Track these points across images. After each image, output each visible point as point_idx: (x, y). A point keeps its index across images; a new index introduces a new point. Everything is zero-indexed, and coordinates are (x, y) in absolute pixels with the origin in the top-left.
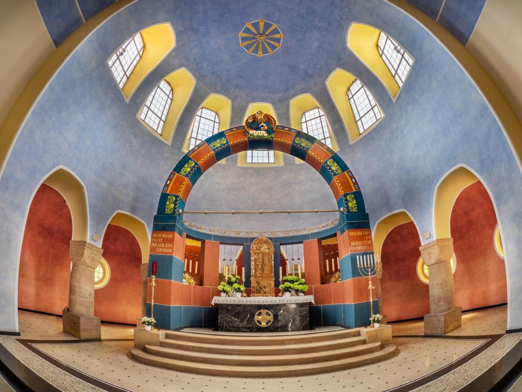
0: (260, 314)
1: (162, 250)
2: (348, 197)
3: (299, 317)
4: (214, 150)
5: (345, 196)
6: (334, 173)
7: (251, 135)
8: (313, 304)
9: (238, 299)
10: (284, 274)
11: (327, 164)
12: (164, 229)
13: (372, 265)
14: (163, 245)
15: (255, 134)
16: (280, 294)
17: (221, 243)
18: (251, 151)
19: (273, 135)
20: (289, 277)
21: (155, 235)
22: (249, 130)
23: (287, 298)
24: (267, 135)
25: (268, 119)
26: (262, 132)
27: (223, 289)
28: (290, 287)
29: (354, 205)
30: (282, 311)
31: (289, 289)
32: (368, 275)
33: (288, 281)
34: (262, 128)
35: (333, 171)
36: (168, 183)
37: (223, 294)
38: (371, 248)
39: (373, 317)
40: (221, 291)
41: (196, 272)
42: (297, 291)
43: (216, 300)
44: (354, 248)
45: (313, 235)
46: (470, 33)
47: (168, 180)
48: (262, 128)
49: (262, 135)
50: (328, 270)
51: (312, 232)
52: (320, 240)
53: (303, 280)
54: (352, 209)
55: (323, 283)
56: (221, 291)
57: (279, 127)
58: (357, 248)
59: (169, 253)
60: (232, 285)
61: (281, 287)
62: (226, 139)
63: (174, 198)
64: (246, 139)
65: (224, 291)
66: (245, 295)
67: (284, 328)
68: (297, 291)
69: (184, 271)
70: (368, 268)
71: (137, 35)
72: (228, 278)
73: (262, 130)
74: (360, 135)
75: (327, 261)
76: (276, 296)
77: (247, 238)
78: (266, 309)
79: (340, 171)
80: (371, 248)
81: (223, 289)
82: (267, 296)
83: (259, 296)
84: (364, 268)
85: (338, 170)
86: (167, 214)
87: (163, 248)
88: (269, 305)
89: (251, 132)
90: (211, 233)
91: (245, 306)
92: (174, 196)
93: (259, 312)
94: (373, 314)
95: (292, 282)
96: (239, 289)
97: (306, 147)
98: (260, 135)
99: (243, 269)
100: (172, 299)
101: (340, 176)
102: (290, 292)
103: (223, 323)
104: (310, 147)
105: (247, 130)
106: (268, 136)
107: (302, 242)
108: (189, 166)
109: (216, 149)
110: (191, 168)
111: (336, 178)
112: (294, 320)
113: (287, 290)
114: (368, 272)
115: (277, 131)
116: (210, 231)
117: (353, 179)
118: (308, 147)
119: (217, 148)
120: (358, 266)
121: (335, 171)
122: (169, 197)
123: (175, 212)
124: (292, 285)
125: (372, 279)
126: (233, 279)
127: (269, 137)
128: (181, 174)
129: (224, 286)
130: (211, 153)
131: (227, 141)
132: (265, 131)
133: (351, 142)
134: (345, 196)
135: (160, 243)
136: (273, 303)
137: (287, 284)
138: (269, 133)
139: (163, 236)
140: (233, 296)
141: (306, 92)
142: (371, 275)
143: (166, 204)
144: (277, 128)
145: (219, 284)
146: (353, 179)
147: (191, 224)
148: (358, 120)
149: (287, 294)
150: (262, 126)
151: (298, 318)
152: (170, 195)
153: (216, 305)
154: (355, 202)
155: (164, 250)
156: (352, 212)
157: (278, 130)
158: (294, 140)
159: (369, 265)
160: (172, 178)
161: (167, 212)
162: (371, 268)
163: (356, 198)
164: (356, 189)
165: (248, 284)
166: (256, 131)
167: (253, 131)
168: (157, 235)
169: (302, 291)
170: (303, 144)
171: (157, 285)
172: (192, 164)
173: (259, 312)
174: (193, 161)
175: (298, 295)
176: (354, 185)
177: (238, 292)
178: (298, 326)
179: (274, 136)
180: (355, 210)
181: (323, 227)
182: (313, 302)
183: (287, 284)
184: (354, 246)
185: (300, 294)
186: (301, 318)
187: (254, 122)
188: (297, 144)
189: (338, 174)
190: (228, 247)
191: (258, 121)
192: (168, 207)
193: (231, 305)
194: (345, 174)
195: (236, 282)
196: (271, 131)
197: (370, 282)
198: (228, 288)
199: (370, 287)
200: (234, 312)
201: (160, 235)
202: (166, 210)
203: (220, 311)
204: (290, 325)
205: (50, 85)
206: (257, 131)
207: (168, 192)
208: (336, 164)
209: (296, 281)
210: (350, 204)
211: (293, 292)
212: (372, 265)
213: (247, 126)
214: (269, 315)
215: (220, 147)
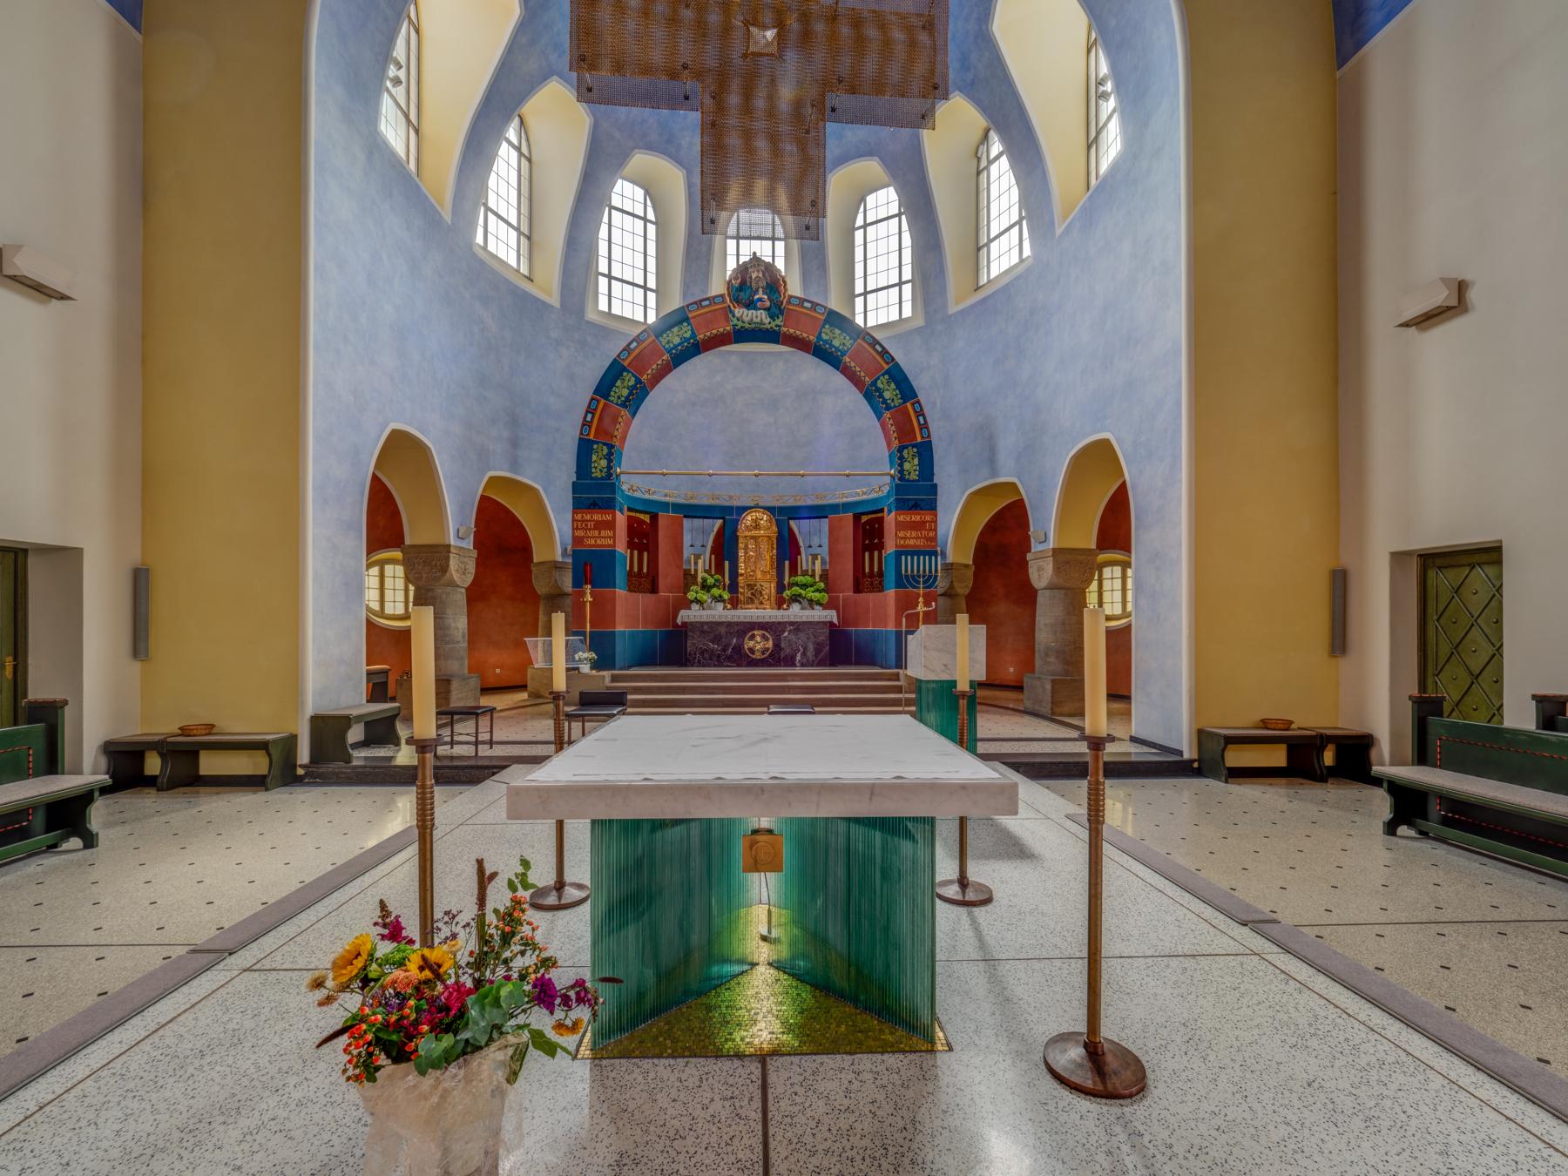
0: (752, 637)
1: (596, 541)
4: (669, 351)
6: (887, 404)
8: (835, 625)
9: (719, 613)
10: (794, 571)
11: (876, 387)
12: (594, 505)
13: (927, 572)
14: (596, 533)
15: (746, 319)
16: (785, 606)
17: (685, 517)
19: (778, 322)
20: (800, 579)
21: (579, 517)
22: (734, 307)
23: (795, 613)
24: (769, 320)
25: (774, 283)
26: (759, 312)
27: (696, 598)
28: (800, 595)
29: (914, 468)
30: (786, 634)
31: (798, 598)
32: (919, 588)
33: (797, 584)
34: (759, 304)
35: (885, 401)
36: (589, 419)
37: (695, 607)
38: (933, 544)
40: (692, 602)
41: (645, 570)
43: (684, 616)
44: (902, 542)
47: (587, 412)
48: (759, 304)
49: (758, 320)
50: (867, 570)
51: (845, 500)
52: (857, 517)
54: (910, 474)
55: (858, 589)
56: (692, 602)
57: (792, 300)
58: (908, 542)
59: (609, 546)
60: (708, 591)
61: (787, 593)
62: (689, 327)
63: (605, 450)
64: (728, 328)
65: (697, 601)
66: (729, 606)
67: (790, 662)
68: (812, 603)
70: (919, 576)
72: (702, 579)
73: (760, 309)
74: (975, 290)
75: (867, 554)
76: (779, 609)
77: (732, 508)
78: (762, 629)
79: (897, 402)
80: (933, 544)
81: (696, 598)
82: (764, 609)
83: (750, 609)
84: (913, 577)
85: (895, 398)
86: (596, 478)
87: (598, 538)
88: (767, 623)
89: (739, 312)
90: (667, 499)
91: (729, 624)
92: (605, 444)
93: (750, 634)
95: (804, 586)
96: (721, 596)
97: (841, 348)
98: (755, 320)
101: (897, 411)
102: (800, 603)
103: (695, 654)
104: (848, 349)
105: (729, 307)
106: (770, 323)
107: (827, 517)
108: (626, 384)
109: (673, 348)
110: (628, 388)
111: (889, 415)
112: (805, 649)
113: (796, 599)
114: (919, 582)
115: (788, 309)
116: (666, 495)
117: (921, 418)
118: (846, 348)
120: (903, 572)
121: (889, 402)
122: (595, 446)
123: (611, 475)
124: (803, 592)
125: (925, 595)
126: (711, 581)
127: (773, 324)
128: (612, 402)
129: (697, 592)
130: (665, 357)
131: (693, 332)
132: (765, 309)
133: (953, 309)
135: (590, 530)
136: (774, 620)
137: (796, 590)
138: (772, 317)
139: (595, 517)
140: (710, 608)
141: (869, 153)
142: (923, 588)
143: (591, 459)
144: (789, 302)
145: (689, 591)
146: (921, 418)
147: (632, 486)
148: (983, 246)
149: (796, 607)
150: (760, 300)
151: (811, 647)
152: (597, 443)
153: (685, 624)
154: (916, 461)
155: (599, 542)
156: (908, 480)
157: (791, 307)
159: (921, 572)
160: (595, 409)
161: (596, 474)
162: (924, 576)
163: (920, 455)
164: (923, 437)
165: (733, 588)
166: (749, 310)
167: (741, 311)
168: (583, 517)
169: (818, 603)
170: (836, 343)
171: (594, 600)
172: (629, 380)
173: (750, 634)
174: (630, 374)
175: (813, 609)
176: (921, 429)
177: (719, 601)
178: (811, 659)
179: (782, 324)
180: (914, 476)
181: (864, 493)
182: (835, 620)
183: (796, 590)
184: (902, 538)
185: (815, 607)
188: (826, 342)
189: (895, 406)
190: (697, 522)
191: (751, 282)
192: (596, 465)
193: (707, 623)
194: (907, 407)
195: (714, 586)
196: (777, 312)
197: (921, 599)
198: (704, 596)
200: (712, 635)
201: (589, 517)
202: (593, 470)
203: (690, 634)
204: (798, 658)
206: (750, 312)
207: (591, 437)
208: (893, 386)
209: (812, 586)
210: (887, 395)
211: (805, 603)
212: (927, 572)
213: (729, 295)
214: (767, 639)
215: (679, 344)
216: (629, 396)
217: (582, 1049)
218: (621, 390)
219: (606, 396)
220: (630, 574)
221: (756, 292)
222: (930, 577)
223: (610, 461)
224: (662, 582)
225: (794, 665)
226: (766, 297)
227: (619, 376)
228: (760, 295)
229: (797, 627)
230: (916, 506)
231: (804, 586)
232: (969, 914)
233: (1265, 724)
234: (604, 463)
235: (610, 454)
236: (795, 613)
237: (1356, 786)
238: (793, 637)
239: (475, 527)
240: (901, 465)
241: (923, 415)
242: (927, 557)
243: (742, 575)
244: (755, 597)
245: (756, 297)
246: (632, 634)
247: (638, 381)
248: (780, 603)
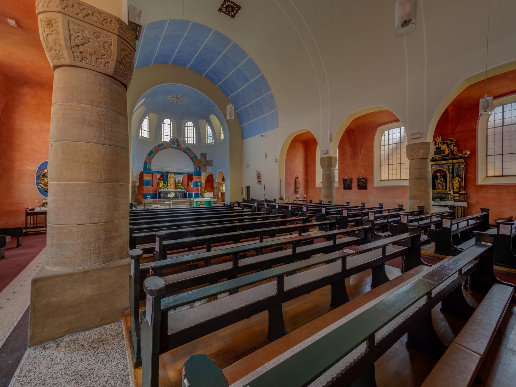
5: (196, 167)
33: (179, 186)
39: (199, 196)
42: (181, 189)
45: (186, 173)
46: (245, 139)
53: (183, 186)
67: (178, 198)
71: (286, 290)
75: (189, 181)
89: (172, 145)
95: (180, 186)
100: (144, 191)
113: (179, 188)
134: (196, 167)
149: (179, 189)
151: (181, 195)
169: (183, 189)
170: (187, 151)
180: (198, 171)
187: (173, 141)
197: (199, 189)
199: (199, 189)
204: (179, 197)
218: (161, 147)
219: (159, 147)
220: (208, 251)
221: (175, 143)
224: (154, 185)
225: (179, 198)
227: (152, 153)
228: (176, 143)
229: (179, 192)
230: (198, 175)
231: (180, 186)
233: (236, 202)
234: (149, 166)
236: (179, 190)
237: (512, 320)
238: (178, 194)
246: (152, 193)
248: (175, 189)
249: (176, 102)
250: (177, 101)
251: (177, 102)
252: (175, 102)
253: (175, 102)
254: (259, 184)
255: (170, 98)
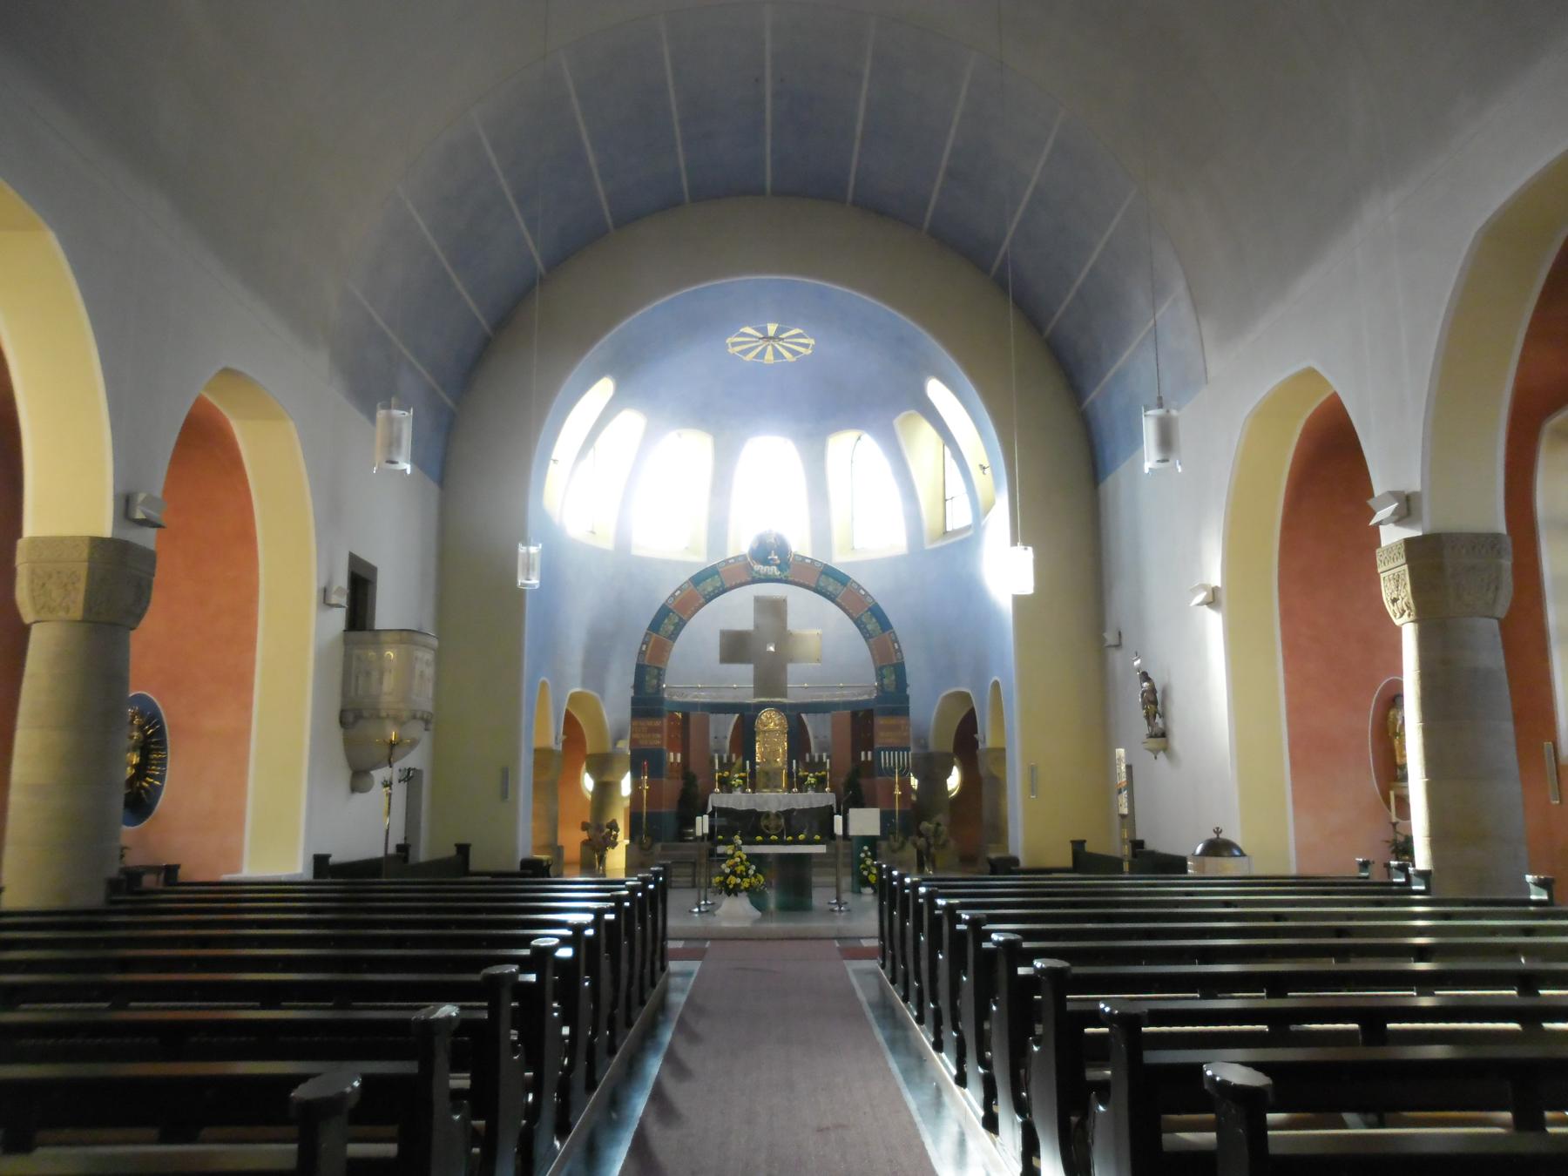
2: (884, 671)
3: (548, 861)
7: (756, 572)
15: (761, 572)
18: (1068, 1003)
36: (644, 649)
47: (643, 644)
48: (771, 562)
69: (1124, 839)
94: (367, 1080)
99: (748, 762)
119: (709, 593)
131: (722, 582)
154: (893, 677)
158: (818, 581)
186: (545, 864)
197: (897, 786)
199: (898, 792)
205: (1382, 1125)
208: (874, 620)
210: (869, 627)
216: (674, 630)
217: (887, 950)
222: (904, 768)
223: (659, 680)
226: (776, 557)
227: (666, 615)
232: (822, 532)
235: (659, 674)
239: (564, 733)
240: (882, 680)
241: (897, 642)
242: (896, 753)
243: (759, 764)
244: (770, 781)
245: (770, 557)
247: (680, 619)
249: (772, 358)
250: (773, 346)
251: (777, 354)
252: (769, 357)
253: (769, 357)
254: (1155, 752)
255: (738, 349)
